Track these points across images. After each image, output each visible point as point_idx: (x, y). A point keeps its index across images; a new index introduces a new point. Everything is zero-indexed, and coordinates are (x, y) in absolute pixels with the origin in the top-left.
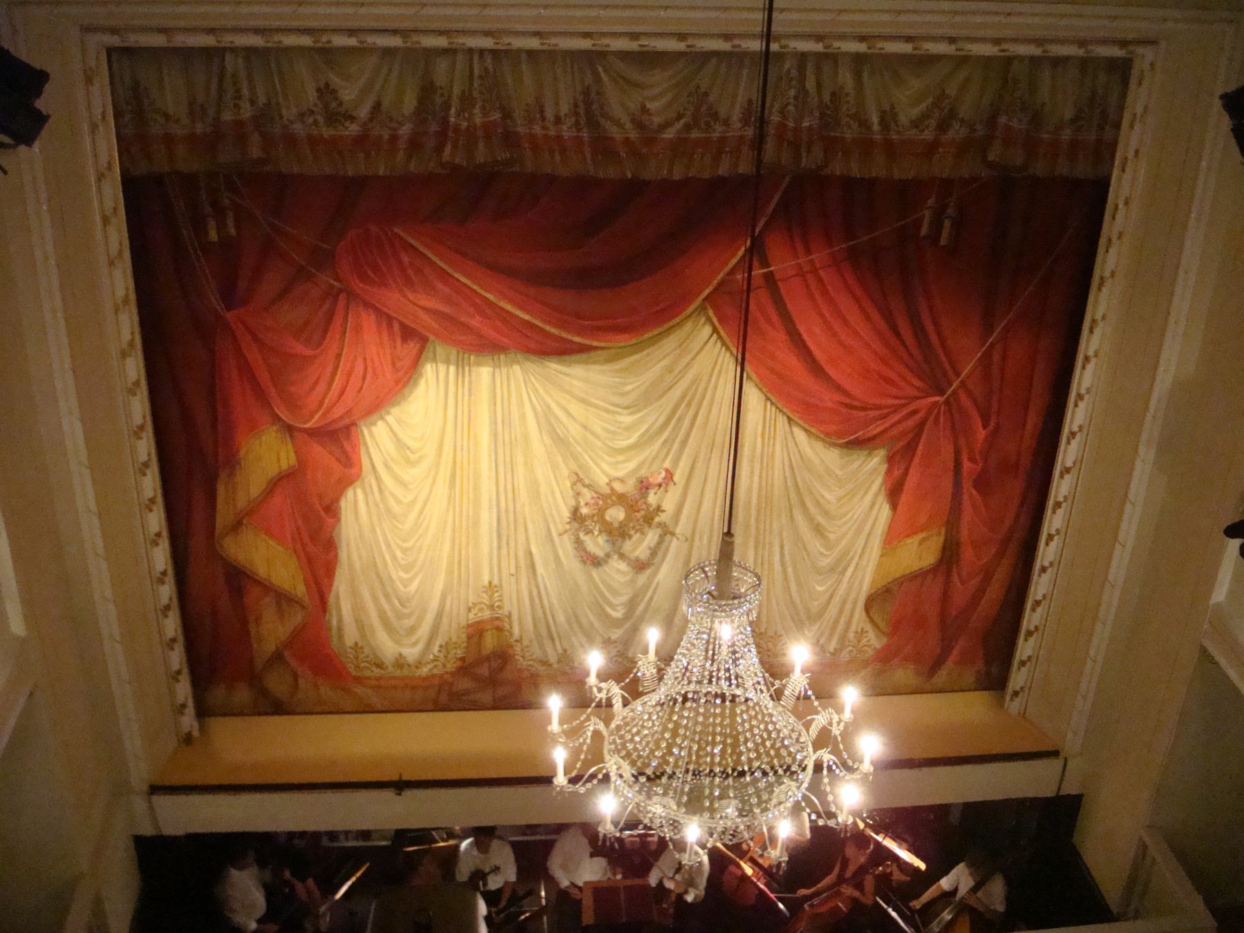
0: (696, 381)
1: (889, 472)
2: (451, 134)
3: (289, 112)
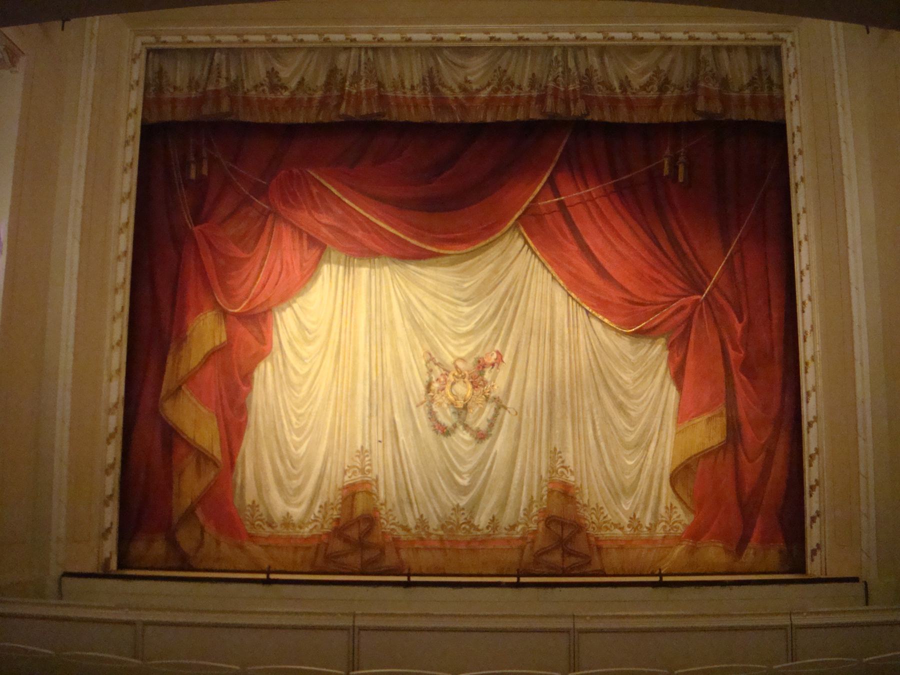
0: (514, 281)
1: (670, 359)
2: (346, 97)
3: (248, 84)
